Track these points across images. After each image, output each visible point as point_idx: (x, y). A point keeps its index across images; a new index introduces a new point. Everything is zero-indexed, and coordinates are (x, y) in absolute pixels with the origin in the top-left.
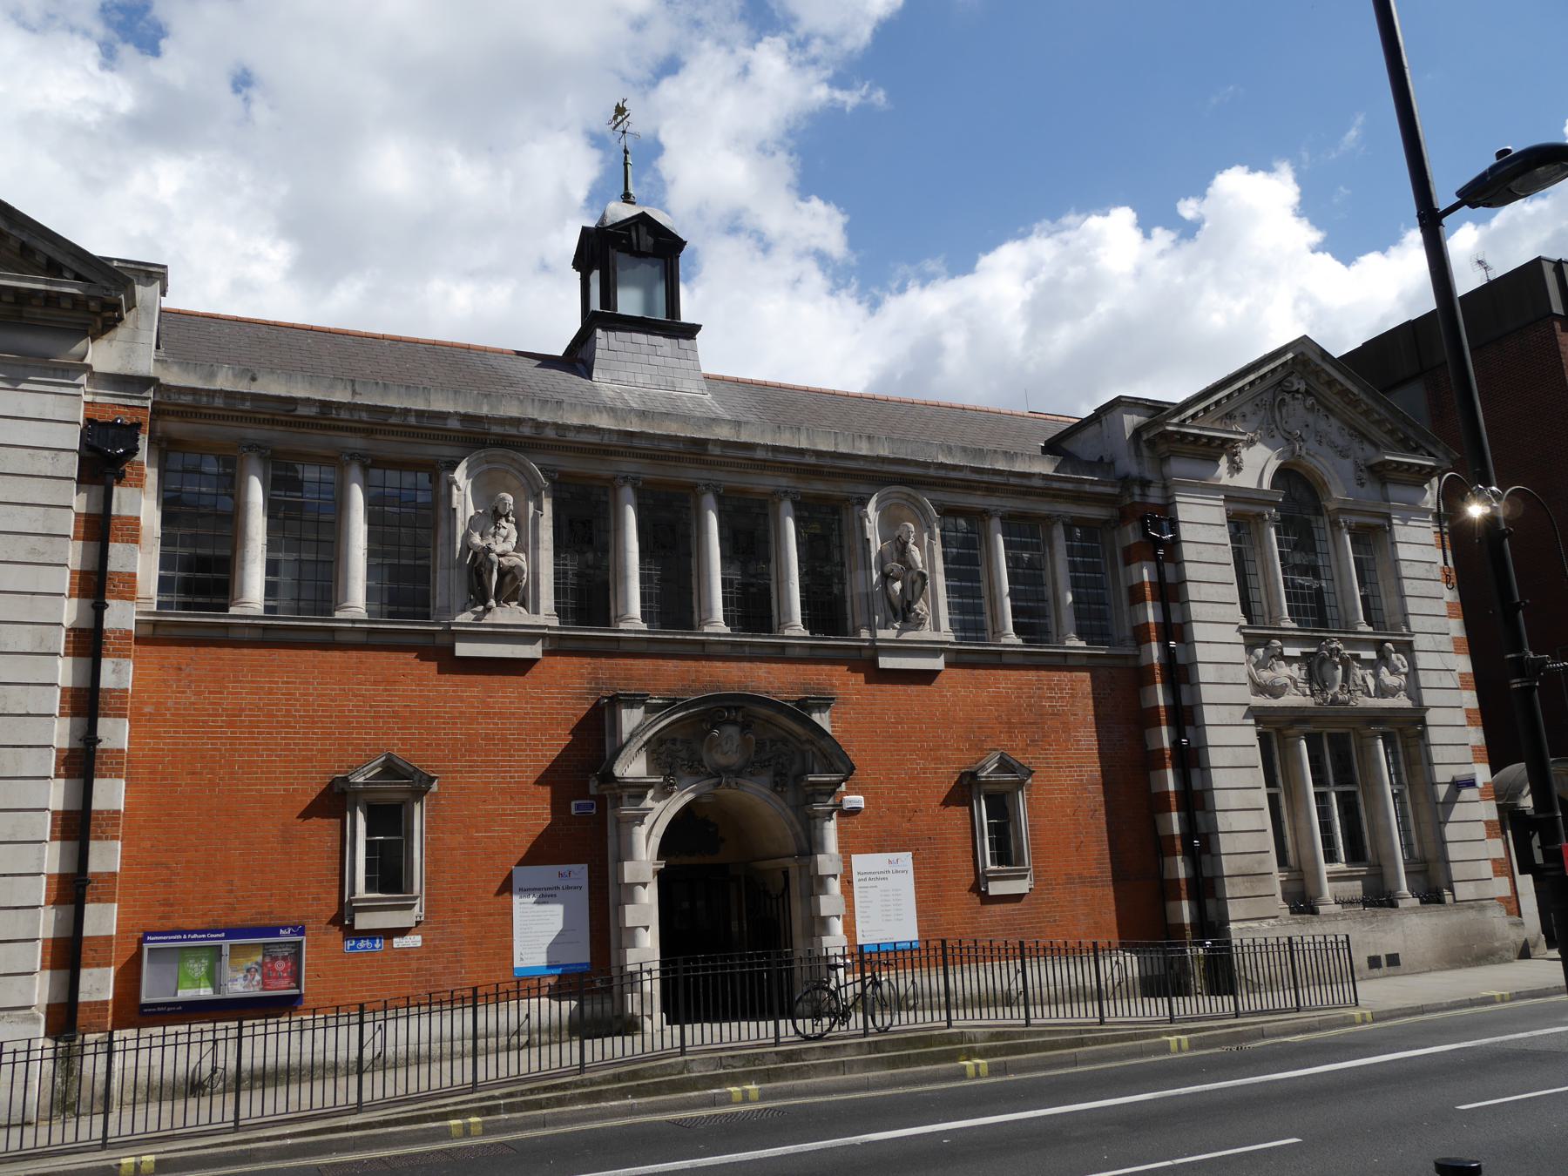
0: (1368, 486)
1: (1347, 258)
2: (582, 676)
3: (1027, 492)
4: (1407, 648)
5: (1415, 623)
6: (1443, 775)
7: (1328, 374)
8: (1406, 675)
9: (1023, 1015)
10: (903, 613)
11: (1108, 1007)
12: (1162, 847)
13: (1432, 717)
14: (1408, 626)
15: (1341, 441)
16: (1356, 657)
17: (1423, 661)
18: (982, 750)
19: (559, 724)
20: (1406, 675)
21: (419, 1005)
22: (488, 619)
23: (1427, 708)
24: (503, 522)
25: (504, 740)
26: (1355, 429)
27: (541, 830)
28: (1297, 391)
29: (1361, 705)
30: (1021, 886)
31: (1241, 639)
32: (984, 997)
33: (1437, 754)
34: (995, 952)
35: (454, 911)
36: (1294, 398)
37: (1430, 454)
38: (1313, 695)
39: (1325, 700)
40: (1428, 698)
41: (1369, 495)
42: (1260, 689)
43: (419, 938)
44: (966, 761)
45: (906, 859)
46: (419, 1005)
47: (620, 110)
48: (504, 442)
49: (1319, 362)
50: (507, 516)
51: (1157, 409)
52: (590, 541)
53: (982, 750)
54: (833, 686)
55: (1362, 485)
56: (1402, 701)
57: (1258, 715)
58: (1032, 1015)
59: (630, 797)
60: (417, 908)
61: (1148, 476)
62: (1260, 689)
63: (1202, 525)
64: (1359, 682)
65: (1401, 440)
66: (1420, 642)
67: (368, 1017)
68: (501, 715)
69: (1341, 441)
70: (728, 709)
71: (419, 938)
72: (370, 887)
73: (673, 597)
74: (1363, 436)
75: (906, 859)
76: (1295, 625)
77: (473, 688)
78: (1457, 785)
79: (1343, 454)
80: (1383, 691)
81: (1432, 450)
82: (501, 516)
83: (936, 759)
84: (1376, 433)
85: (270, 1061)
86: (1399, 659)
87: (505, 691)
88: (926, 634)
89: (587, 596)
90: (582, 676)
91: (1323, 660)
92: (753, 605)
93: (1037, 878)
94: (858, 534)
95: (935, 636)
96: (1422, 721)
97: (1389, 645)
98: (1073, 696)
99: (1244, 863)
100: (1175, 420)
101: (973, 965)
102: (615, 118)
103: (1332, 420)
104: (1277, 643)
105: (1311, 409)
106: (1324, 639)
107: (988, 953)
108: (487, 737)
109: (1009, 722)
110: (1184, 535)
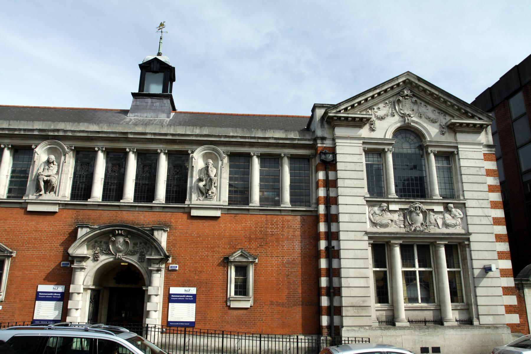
0: (447, 134)
1: (174, 68)
2: (72, 218)
3: (269, 145)
4: (463, 206)
5: (467, 195)
6: (477, 266)
7: (423, 87)
8: (461, 219)
10: (205, 193)
12: (318, 292)
13: (472, 238)
14: (463, 196)
15: (432, 116)
16: (432, 210)
17: (470, 212)
19: (61, 235)
20: (461, 219)
21: (219, 334)
22: (41, 198)
23: (470, 234)
24: (52, 165)
25: (41, 240)
26: (441, 110)
27: (49, 271)
28: (407, 95)
29: (432, 231)
30: (247, 305)
31: (365, 203)
33: (475, 255)
35: (15, 298)
36: (405, 99)
37: (480, 119)
38: (405, 227)
39: (411, 230)
40: (471, 229)
41: (448, 138)
42: (374, 224)
44: (228, 251)
46: (219, 334)
49: (417, 82)
50: (53, 162)
51: (328, 107)
53: (235, 248)
54: (171, 222)
55: (443, 134)
56: (459, 230)
57: (371, 236)
59: (77, 261)
60: (251, 301)
61: (326, 135)
62: (374, 224)
63: (350, 156)
64: (433, 221)
65: (464, 113)
66: (468, 203)
67: (262, 339)
68: (41, 231)
69: (432, 116)
70: (118, 230)
72: (236, 293)
73: (114, 188)
74: (445, 113)
76: (397, 197)
77: (33, 221)
78: (487, 269)
79: (433, 121)
80: (446, 225)
81: (481, 117)
82: (50, 163)
83: (213, 252)
84: (450, 110)
85: (277, 348)
86: (457, 212)
87: (44, 224)
88: (214, 202)
90: (72, 218)
91: (411, 212)
92: (145, 191)
93: (255, 301)
94: (190, 164)
95: (218, 203)
96: (468, 239)
97: (452, 205)
98: (283, 227)
99: (355, 301)
100: (334, 111)
103: (429, 107)
104: (385, 204)
105: (415, 103)
106: (413, 202)
108: (35, 239)
109: (250, 238)
110: (338, 159)
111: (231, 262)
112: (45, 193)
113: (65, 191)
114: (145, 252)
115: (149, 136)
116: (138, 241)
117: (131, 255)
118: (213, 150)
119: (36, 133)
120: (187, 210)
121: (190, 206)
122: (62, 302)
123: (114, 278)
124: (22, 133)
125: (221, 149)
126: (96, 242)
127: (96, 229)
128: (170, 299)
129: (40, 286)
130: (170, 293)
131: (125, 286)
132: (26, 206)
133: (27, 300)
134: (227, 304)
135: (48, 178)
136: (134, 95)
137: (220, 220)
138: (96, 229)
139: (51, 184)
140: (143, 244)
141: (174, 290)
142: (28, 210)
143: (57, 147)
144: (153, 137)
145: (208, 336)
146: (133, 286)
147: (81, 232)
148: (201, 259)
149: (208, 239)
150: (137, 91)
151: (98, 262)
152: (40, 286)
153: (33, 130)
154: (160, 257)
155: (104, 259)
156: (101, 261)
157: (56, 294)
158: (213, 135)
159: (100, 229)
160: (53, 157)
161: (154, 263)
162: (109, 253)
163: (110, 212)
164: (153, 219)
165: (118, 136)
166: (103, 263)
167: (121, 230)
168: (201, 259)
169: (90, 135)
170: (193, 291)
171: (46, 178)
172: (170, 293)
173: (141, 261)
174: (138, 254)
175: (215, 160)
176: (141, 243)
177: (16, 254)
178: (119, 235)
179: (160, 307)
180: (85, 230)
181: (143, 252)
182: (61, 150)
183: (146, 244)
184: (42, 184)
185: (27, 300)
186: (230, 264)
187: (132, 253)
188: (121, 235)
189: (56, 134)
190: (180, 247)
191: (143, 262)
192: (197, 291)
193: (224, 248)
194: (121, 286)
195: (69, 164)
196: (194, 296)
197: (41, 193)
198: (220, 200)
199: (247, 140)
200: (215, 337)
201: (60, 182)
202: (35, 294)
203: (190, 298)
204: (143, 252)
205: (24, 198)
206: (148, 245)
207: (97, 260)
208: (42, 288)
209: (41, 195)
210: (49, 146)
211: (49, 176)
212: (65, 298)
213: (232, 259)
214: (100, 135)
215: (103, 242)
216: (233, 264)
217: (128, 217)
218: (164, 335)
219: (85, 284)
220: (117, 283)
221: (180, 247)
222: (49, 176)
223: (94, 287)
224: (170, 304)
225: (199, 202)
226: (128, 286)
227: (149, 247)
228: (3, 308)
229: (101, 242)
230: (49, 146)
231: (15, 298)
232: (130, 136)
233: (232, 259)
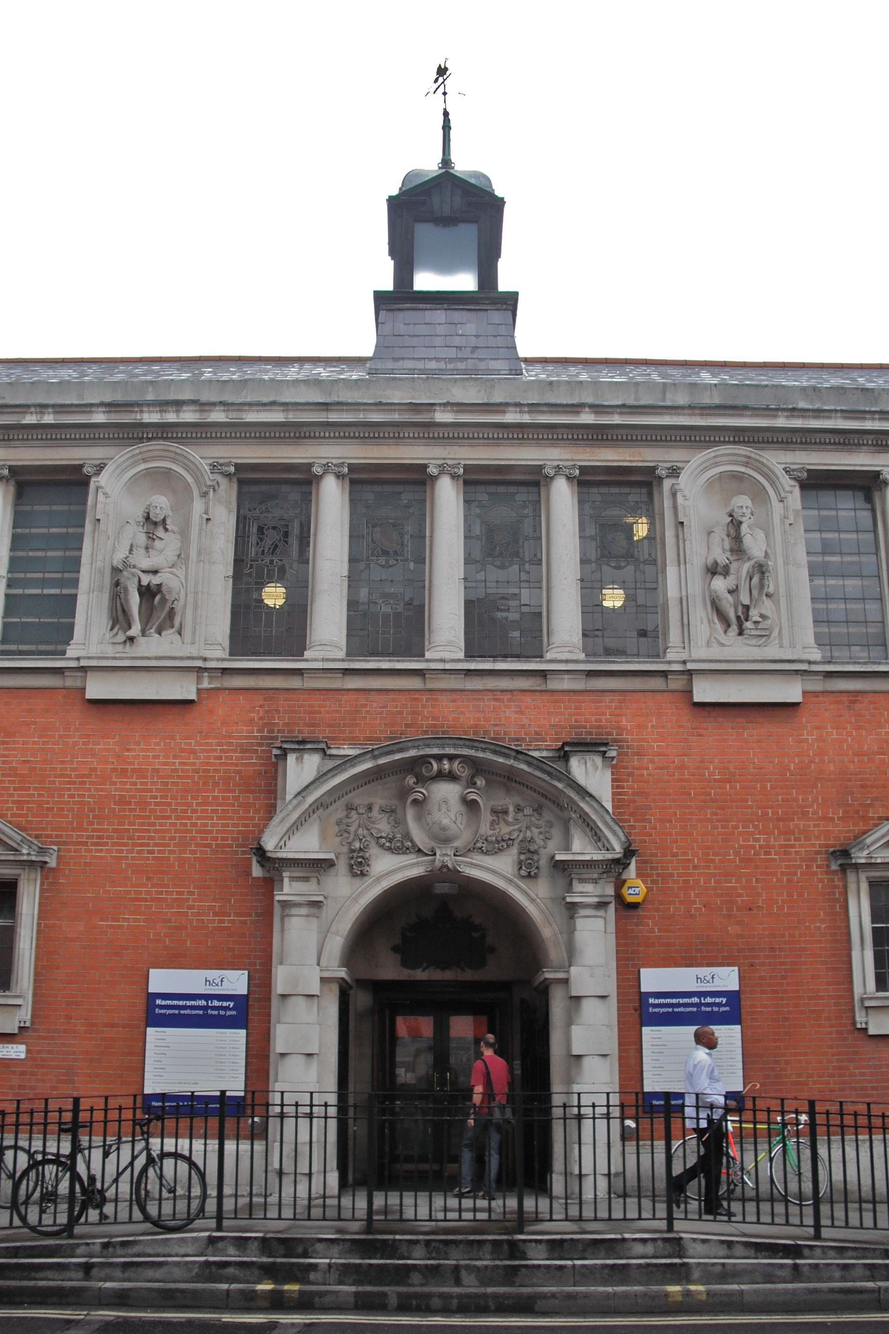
1: (503, 198)
9: (809, 1220)
11: (472, 1206)
18: (865, 819)
24: (160, 532)
25: (143, 804)
32: (646, 1183)
34: (849, 1120)
35: (68, 1017)
43: (23, 1048)
44: (839, 832)
45: (736, 969)
47: (442, 71)
48: (164, 431)
52: (121, 571)
53: (865, 819)
58: (825, 1221)
59: (292, 879)
68: (141, 773)
70: (439, 758)
71: (23, 1048)
75: (736, 969)
77: (108, 743)
83: (787, 833)
87: (150, 749)
89: (269, 632)
101: (836, 1138)
102: (436, 81)
107: (835, 1120)
108: (122, 801)
111: (857, 867)
112: (144, 633)
113: (208, 626)
114: (539, 841)
115: (511, 417)
116: (509, 802)
117: (486, 853)
118: (746, 465)
119: (99, 417)
120: (676, 684)
121: (690, 666)
122: (243, 1032)
123: (395, 949)
124: (49, 419)
125: (777, 460)
126: (350, 808)
127: (352, 761)
128: (641, 1012)
129: (154, 973)
130: (644, 989)
131: (437, 975)
132: (78, 684)
133: (114, 1026)
134: (854, 1023)
135: (156, 580)
136: (380, 298)
137: (803, 717)
138: (352, 761)
139: (164, 600)
140: (528, 811)
141: (653, 979)
142: (89, 696)
143: (174, 467)
144: (526, 418)
145: (324, 1197)
146: (469, 975)
147: (300, 771)
148: (746, 861)
149: (764, 787)
150: (387, 284)
151: (368, 881)
152: (154, 973)
153: (88, 408)
154: (610, 856)
155: (390, 870)
156: (378, 879)
157: (216, 1003)
158: (746, 408)
159: (375, 757)
160: (161, 503)
161: (582, 881)
162: (401, 845)
163: (391, 696)
164: (554, 720)
165: (396, 417)
166: (386, 884)
167: (451, 758)
168: (746, 861)
169: (292, 417)
170: (727, 978)
171: (146, 580)
172: (644, 989)
173: (529, 876)
174: (514, 851)
175: (759, 496)
176: (519, 809)
177: (59, 858)
178: (441, 776)
179: (611, 1043)
180: (312, 763)
181: (531, 841)
182: (190, 479)
183: (538, 810)
184: (134, 599)
185: (114, 1026)
186: (851, 877)
187: (497, 847)
188: (452, 777)
189: (171, 417)
190: (662, 821)
191: (536, 876)
192: (741, 979)
193: (824, 818)
194: (420, 975)
195: (216, 527)
196: (733, 997)
197: (131, 633)
198: (793, 646)
199: (869, 425)
200: (324, 1197)
201: (86, 631)
202: (141, 1001)
203: (719, 1005)
204: (531, 841)
205: (70, 653)
206: (547, 815)
207: (363, 874)
208: (162, 980)
209: (131, 639)
210: (143, 466)
211: (155, 572)
212: (249, 1013)
213: (860, 857)
214: (334, 417)
215: (376, 809)
216: (863, 877)
217: (464, 715)
218: (631, 1147)
219: (324, 963)
220: (406, 963)
221: (662, 821)
222: (155, 572)
223: (342, 973)
224: (644, 1028)
225: (715, 652)
226: (448, 975)
227: (550, 824)
228: (28, 1051)
229: (370, 808)
230: (143, 466)
231: (68, 1017)
232: (442, 417)
233: (860, 857)
